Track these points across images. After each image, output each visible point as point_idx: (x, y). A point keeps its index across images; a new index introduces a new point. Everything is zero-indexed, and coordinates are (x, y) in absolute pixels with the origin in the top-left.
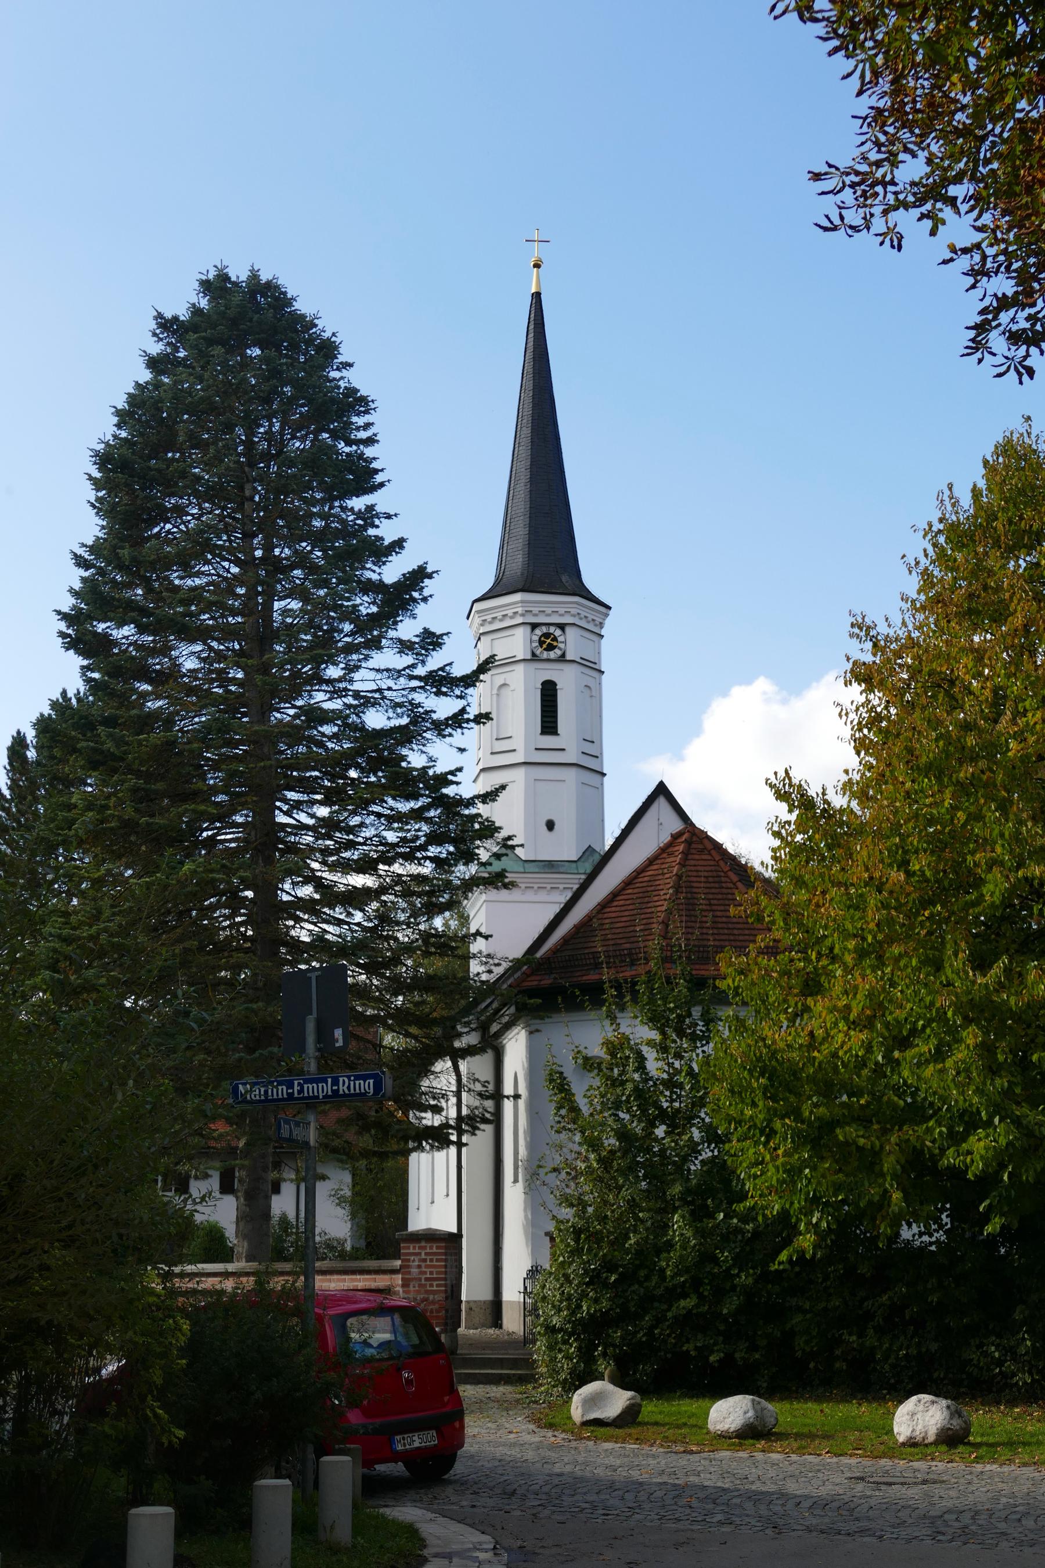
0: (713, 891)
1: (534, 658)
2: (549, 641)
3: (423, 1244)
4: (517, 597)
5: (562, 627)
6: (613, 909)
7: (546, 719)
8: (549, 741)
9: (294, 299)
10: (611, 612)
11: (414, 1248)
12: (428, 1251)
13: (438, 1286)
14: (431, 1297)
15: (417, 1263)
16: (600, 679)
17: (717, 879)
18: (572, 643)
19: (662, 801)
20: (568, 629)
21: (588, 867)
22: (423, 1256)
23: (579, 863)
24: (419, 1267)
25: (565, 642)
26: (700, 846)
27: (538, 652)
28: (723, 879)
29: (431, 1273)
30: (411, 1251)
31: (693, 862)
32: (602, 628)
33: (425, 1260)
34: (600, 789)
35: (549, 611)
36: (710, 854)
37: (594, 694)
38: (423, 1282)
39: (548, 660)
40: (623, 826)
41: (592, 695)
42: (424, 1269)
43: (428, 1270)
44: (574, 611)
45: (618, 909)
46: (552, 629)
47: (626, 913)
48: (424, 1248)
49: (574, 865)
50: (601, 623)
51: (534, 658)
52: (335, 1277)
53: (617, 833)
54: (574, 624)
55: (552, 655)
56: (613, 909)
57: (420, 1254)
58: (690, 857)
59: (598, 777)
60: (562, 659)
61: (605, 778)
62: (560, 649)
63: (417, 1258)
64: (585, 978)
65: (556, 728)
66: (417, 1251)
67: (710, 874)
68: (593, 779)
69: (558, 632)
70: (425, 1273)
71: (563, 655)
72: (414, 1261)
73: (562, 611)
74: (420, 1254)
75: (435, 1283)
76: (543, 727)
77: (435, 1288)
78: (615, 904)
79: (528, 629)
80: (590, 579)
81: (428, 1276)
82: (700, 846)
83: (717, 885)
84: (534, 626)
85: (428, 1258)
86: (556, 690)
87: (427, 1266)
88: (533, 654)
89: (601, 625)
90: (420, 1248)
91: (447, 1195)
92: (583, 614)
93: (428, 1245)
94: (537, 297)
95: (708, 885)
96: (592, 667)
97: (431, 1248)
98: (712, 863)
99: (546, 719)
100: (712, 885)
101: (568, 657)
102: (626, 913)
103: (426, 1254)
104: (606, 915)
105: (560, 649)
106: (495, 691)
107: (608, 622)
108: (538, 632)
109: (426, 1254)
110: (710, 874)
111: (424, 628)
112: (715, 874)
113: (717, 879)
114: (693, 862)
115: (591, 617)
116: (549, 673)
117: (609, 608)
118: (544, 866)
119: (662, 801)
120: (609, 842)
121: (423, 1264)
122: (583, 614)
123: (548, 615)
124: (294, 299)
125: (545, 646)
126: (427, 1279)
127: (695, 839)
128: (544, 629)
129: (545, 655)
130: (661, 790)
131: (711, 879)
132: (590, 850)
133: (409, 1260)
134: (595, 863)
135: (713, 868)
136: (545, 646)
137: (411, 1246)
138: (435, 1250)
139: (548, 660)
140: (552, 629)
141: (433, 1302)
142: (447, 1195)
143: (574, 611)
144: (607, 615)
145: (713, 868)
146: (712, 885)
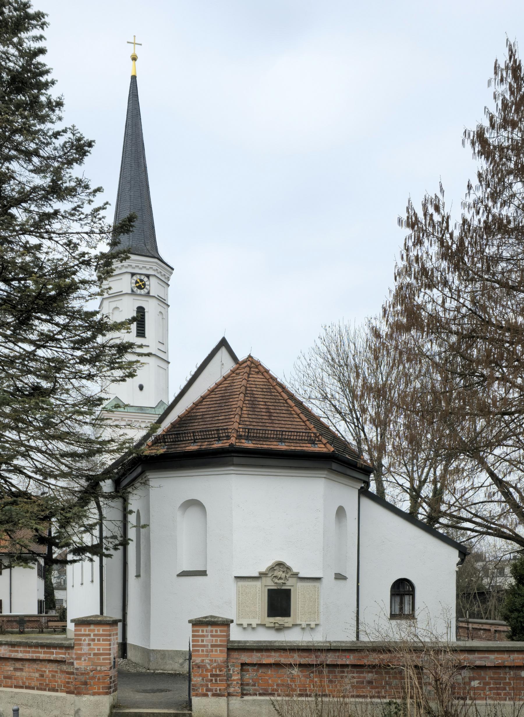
0: (267, 397)
1: (133, 293)
2: (141, 283)
3: (92, 627)
5: (148, 276)
6: (203, 407)
10: (174, 272)
11: (85, 630)
12: (96, 633)
13: (104, 659)
14: (99, 668)
15: (87, 642)
16: (167, 309)
17: (268, 390)
18: (153, 286)
19: (223, 351)
20: (151, 278)
21: (161, 411)
22: (92, 637)
23: (156, 409)
24: (89, 645)
25: (149, 285)
26: (257, 370)
27: (135, 289)
28: (272, 390)
29: (99, 649)
30: (83, 633)
31: (252, 379)
32: (169, 280)
33: (93, 640)
34: (166, 370)
35: (141, 266)
36: (263, 375)
37: (164, 317)
38: (92, 656)
39: (140, 295)
40: (193, 373)
41: (163, 316)
42: (92, 647)
43: (96, 647)
44: (155, 268)
45: (207, 406)
47: (212, 409)
48: (94, 631)
49: (153, 410)
50: (168, 278)
51: (133, 293)
52: (22, 649)
53: (178, 392)
54: (155, 276)
55: (143, 292)
56: (203, 407)
57: (89, 635)
58: (251, 376)
59: (166, 363)
60: (148, 294)
61: (170, 365)
62: (147, 289)
63: (87, 638)
64: (187, 448)
65: (144, 334)
66: (87, 633)
67: (264, 387)
68: (163, 364)
69: (146, 279)
70: (94, 649)
71: (149, 293)
72: (85, 640)
73: (148, 267)
75: (102, 657)
76: (137, 333)
78: (204, 403)
80: (162, 252)
81: (96, 651)
82: (257, 370)
83: (269, 394)
84: (133, 274)
85: (96, 638)
86: (144, 313)
88: (132, 291)
89: (168, 279)
90: (89, 630)
91: (92, 581)
92: (159, 270)
93: (96, 629)
94: (134, 78)
95: (264, 393)
96: (163, 302)
97: (98, 630)
98: (265, 380)
100: (266, 393)
101: (151, 294)
102: (212, 409)
103: (95, 635)
104: (198, 411)
105: (147, 289)
107: (172, 277)
108: (135, 278)
109: (95, 635)
110: (264, 387)
112: (267, 387)
113: (268, 390)
114: (252, 379)
115: (163, 273)
117: (173, 269)
118: (138, 409)
119: (223, 351)
120: (171, 399)
121: (92, 643)
122: (159, 270)
123: (141, 269)
125: (137, 285)
126: (95, 654)
127: (253, 365)
128: (138, 276)
129: (139, 291)
130: (223, 343)
131: (265, 390)
132: (161, 403)
133: (81, 640)
134: (165, 408)
135: (266, 383)
136: (137, 285)
137: (83, 629)
138: (101, 632)
139: (140, 295)
141: (100, 672)
142: (92, 581)
143: (155, 268)
144: (171, 273)
145: (266, 383)
146: (266, 393)
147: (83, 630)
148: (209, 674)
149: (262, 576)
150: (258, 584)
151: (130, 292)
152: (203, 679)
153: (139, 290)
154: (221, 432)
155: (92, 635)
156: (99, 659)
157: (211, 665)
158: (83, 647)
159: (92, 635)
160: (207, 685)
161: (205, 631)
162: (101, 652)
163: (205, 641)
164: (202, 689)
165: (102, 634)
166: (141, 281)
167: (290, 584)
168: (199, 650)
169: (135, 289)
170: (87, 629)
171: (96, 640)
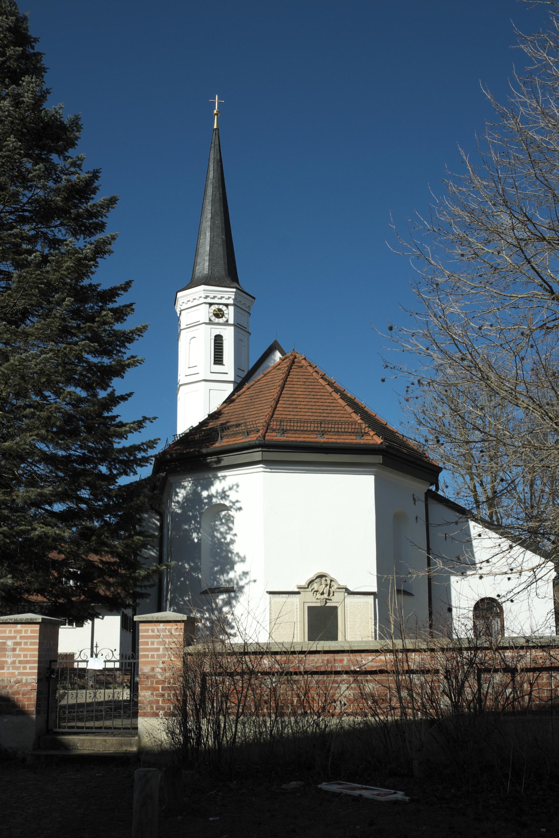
1: (211, 323)
4: (203, 287)
7: (216, 350)
8: (218, 368)
9: (36, 40)
12: (23, 634)
22: (18, 640)
29: (25, 656)
30: (7, 634)
32: (250, 309)
43: (22, 653)
46: (221, 307)
50: (249, 306)
55: (221, 320)
62: (226, 318)
65: (222, 361)
66: (13, 634)
69: (224, 308)
70: (19, 656)
71: (227, 321)
74: (15, 637)
75: (28, 666)
76: (215, 361)
77: (28, 671)
79: (208, 306)
81: (22, 659)
84: (211, 304)
85: (23, 641)
87: (21, 650)
88: (210, 320)
90: (16, 632)
97: (26, 632)
99: (216, 350)
105: (226, 318)
106: (188, 341)
108: (214, 307)
109: (21, 637)
111: (76, 124)
116: (217, 330)
124: (36, 40)
126: (20, 662)
128: (217, 306)
129: (217, 320)
138: (29, 634)
140: (221, 307)
141: (26, 684)
147: (8, 631)
148: (160, 686)
149: (300, 590)
150: (295, 599)
151: (208, 321)
152: (152, 694)
153: (217, 319)
154: (248, 424)
155: (18, 637)
156: (25, 668)
157: (162, 676)
158: (7, 653)
159: (18, 637)
160: (158, 701)
161: (156, 631)
162: (28, 659)
163: (155, 643)
164: (152, 708)
165: (30, 636)
166: (220, 310)
167: (336, 600)
168: (148, 655)
169: (213, 318)
170: (13, 629)
171: (23, 643)
